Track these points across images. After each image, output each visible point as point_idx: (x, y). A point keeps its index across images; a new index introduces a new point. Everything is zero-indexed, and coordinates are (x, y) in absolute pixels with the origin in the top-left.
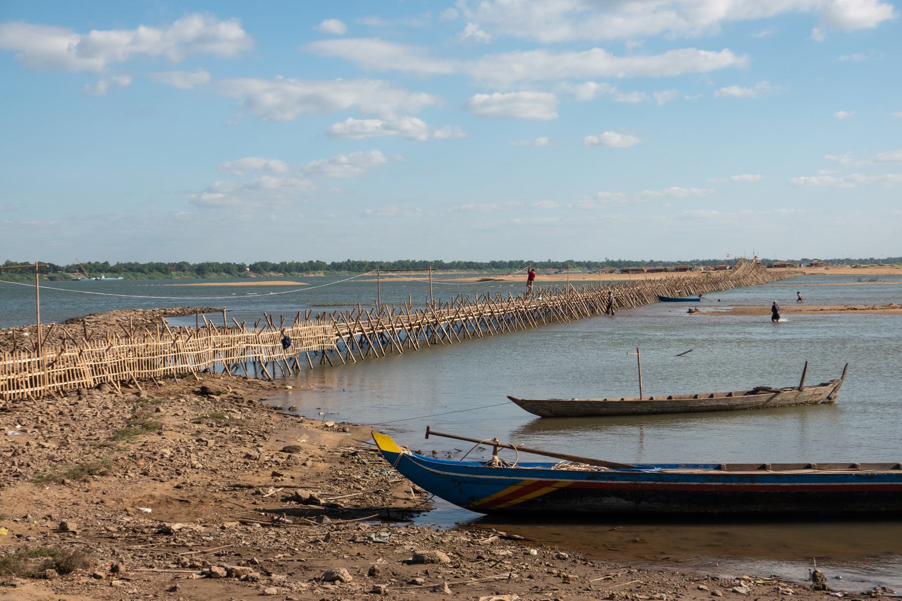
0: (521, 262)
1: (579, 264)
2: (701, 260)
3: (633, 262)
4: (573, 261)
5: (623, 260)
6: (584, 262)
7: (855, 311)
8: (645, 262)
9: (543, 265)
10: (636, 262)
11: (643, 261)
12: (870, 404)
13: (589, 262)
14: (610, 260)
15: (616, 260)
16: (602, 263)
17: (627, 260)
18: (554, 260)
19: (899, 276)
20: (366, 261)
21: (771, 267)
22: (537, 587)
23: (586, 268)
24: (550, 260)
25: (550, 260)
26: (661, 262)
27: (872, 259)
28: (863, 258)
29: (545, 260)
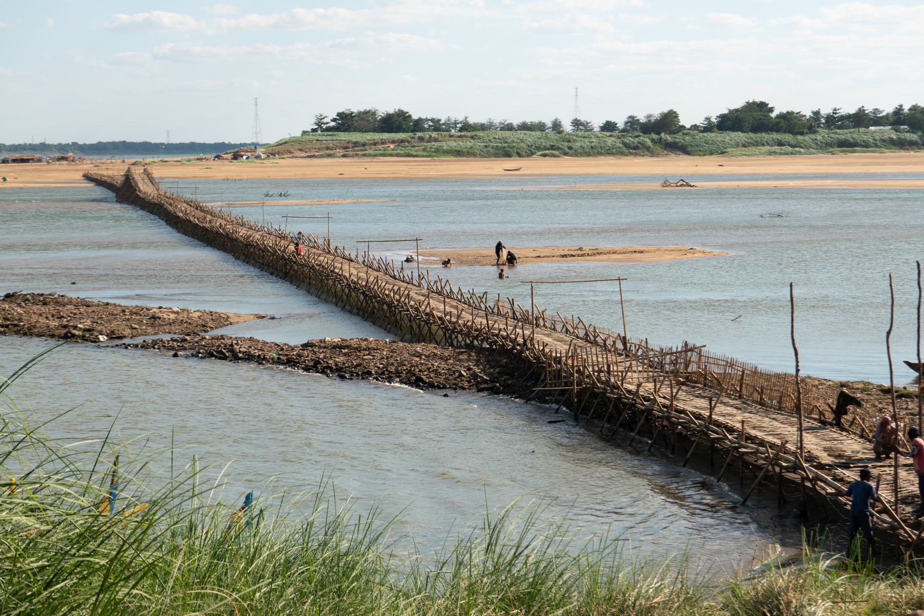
27: (75, 144)
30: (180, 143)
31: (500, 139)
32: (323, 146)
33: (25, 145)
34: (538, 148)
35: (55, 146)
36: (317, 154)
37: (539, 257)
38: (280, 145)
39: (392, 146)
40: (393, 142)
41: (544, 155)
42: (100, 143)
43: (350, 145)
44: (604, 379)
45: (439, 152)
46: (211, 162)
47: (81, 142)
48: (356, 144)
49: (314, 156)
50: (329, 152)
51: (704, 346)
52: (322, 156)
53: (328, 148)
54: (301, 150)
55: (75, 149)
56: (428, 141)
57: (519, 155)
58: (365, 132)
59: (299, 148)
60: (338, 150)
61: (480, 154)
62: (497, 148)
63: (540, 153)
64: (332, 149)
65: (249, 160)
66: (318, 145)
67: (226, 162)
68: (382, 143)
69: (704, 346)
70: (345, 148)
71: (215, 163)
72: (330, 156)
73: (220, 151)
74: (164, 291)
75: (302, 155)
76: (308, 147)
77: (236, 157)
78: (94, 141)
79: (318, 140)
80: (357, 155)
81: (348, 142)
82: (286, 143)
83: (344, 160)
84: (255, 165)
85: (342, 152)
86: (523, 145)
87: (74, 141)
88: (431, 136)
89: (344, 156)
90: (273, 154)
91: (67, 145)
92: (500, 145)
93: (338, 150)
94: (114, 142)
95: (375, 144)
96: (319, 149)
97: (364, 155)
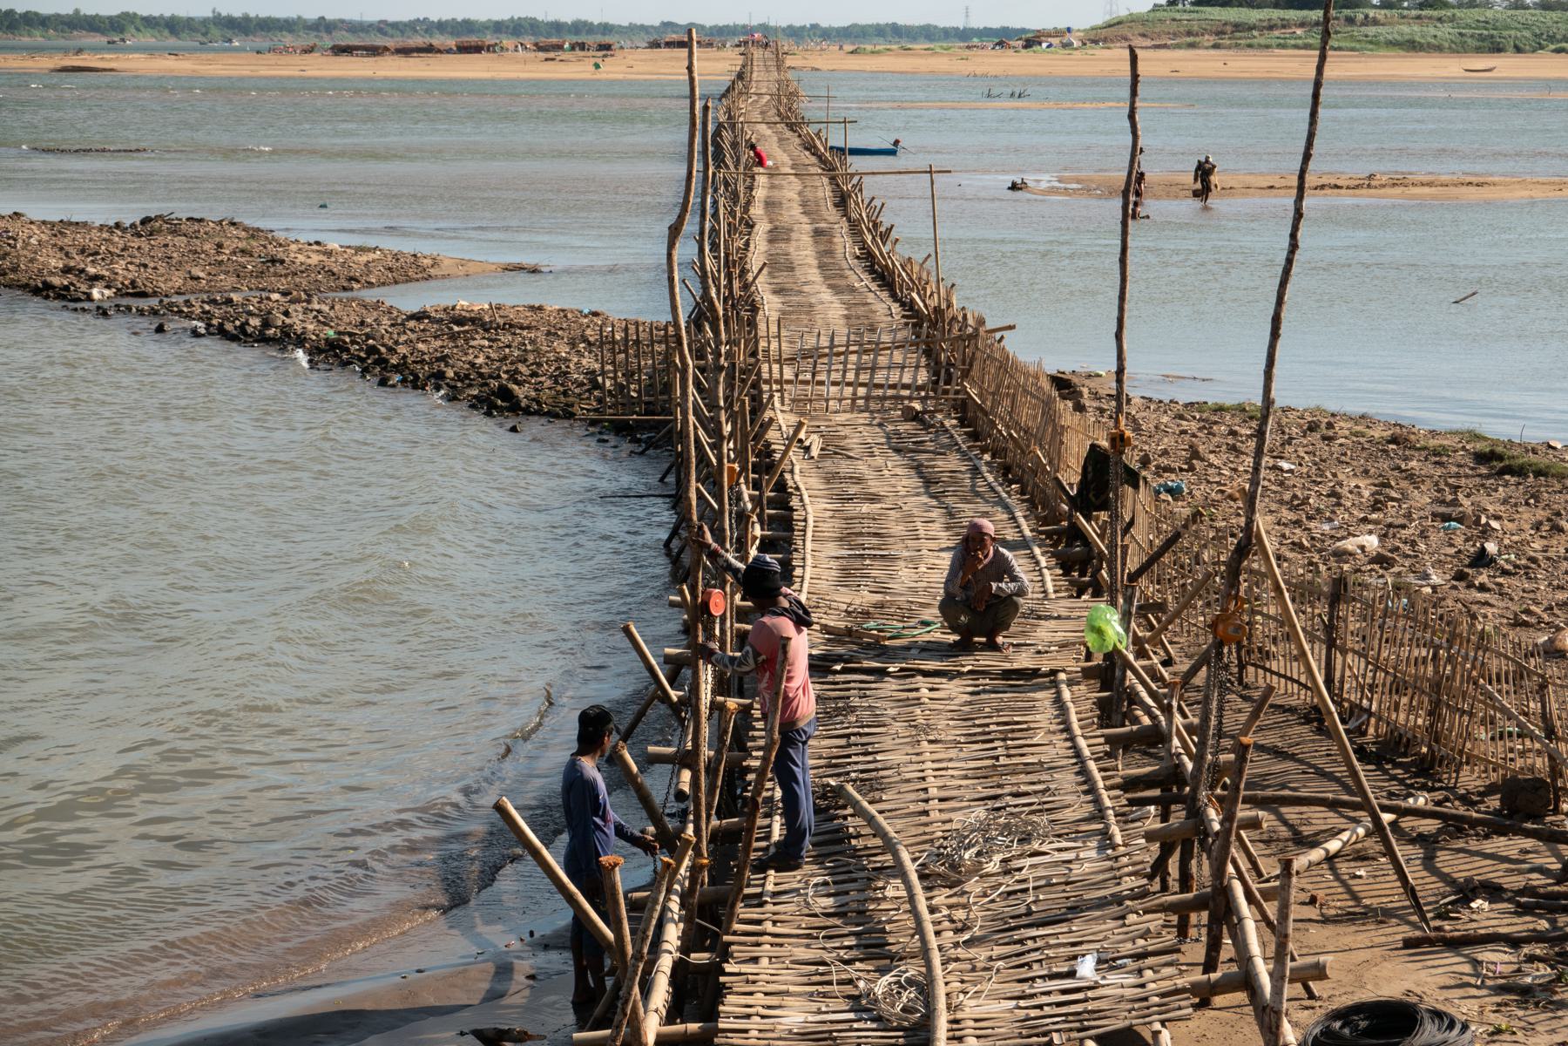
0: (10, 13)
1: (150, 23)
2: (20, 10)
3: (278, 20)
4: (135, 14)
5: (252, 15)
6: (161, 17)
7: (1336, 191)
8: (305, 21)
9: (63, 23)
10: (286, 21)
11: (299, 18)
12: (542, 718)
13: (173, 18)
14: (224, 14)
15: (237, 13)
16: (205, 21)
17: (263, 14)
18: (89, 10)
19: (1565, 422)
20: (489, 21)
21: (1497, 49)
22: (596, 314)
23: (166, 32)
24: (77, 11)
25: (77, 11)
26: (342, 21)
27: (815, 27)
28: (797, 24)
29: (66, 9)
30: (985, 28)
31: (1487, 22)
32: (1182, 29)
33: (736, 26)
34: (1552, 39)
35: (784, 30)
36: (1170, 42)
37: (1272, 187)
38: (1110, 26)
39: (1299, 32)
40: (1302, 25)
41: (1558, 51)
42: (854, 26)
43: (1229, 29)
44: (634, 394)
45: (1374, 43)
46: (989, 52)
47: (824, 24)
48: (1238, 27)
49: (1165, 46)
50: (1190, 39)
51: (1011, 328)
52: (1178, 46)
53: (1189, 33)
54: (1144, 35)
55: (815, 35)
56: (1363, 24)
57: (1518, 50)
58: (1253, 7)
59: (1141, 31)
60: (1207, 37)
61: (1450, 48)
62: (1481, 38)
63: (1553, 47)
64: (1197, 35)
65: (1052, 49)
66: (1174, 27)
67: (1010, 52)
68: (1284, 27)
69: (1011, 328)
70: (1220, 33)
71: (993, 52)
72: (1192, 46)
73: (1002, 38)
74: (431, 224)
75: (1144, 44)
76: (1157, 30)
77: (1029, 44)
78: (845, 23)
79: (1174, 20)
80: (1237, 46)
81: (1225, 24)
82: (1119, 23)
83: (1212, 52)
84: (1057, 56)
85: (1212, 39)
86: (1527, 34)
87: (813, 22)
88: (1367, 17)
89: (1216, 46)
90: (1095, 42)
91: (803, 28)
92: (1485, 32)
93: (1207, 37)
94: (878, 25)
95: (1271, 28)
96: (1175, 34)
97: (1250, 46)
